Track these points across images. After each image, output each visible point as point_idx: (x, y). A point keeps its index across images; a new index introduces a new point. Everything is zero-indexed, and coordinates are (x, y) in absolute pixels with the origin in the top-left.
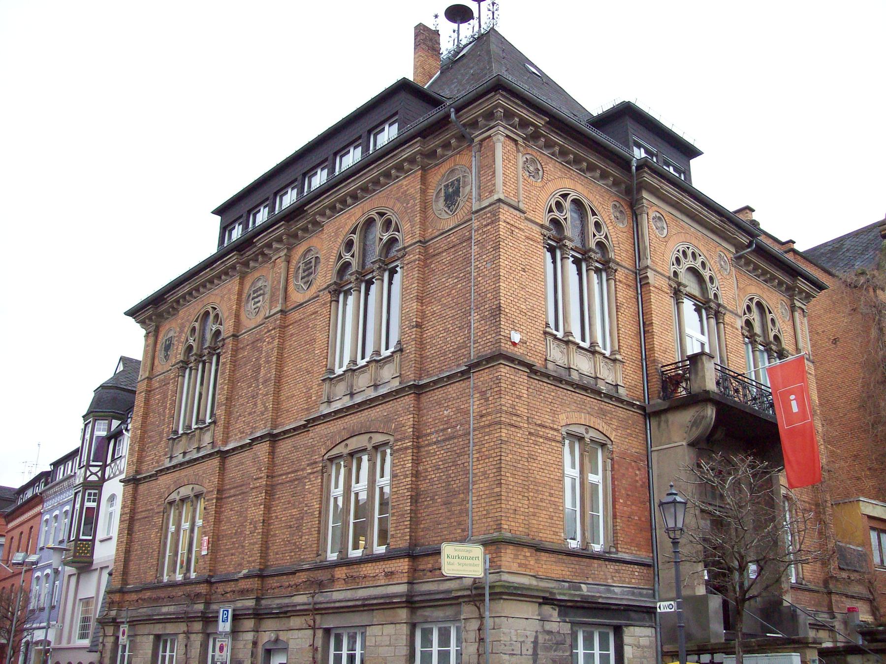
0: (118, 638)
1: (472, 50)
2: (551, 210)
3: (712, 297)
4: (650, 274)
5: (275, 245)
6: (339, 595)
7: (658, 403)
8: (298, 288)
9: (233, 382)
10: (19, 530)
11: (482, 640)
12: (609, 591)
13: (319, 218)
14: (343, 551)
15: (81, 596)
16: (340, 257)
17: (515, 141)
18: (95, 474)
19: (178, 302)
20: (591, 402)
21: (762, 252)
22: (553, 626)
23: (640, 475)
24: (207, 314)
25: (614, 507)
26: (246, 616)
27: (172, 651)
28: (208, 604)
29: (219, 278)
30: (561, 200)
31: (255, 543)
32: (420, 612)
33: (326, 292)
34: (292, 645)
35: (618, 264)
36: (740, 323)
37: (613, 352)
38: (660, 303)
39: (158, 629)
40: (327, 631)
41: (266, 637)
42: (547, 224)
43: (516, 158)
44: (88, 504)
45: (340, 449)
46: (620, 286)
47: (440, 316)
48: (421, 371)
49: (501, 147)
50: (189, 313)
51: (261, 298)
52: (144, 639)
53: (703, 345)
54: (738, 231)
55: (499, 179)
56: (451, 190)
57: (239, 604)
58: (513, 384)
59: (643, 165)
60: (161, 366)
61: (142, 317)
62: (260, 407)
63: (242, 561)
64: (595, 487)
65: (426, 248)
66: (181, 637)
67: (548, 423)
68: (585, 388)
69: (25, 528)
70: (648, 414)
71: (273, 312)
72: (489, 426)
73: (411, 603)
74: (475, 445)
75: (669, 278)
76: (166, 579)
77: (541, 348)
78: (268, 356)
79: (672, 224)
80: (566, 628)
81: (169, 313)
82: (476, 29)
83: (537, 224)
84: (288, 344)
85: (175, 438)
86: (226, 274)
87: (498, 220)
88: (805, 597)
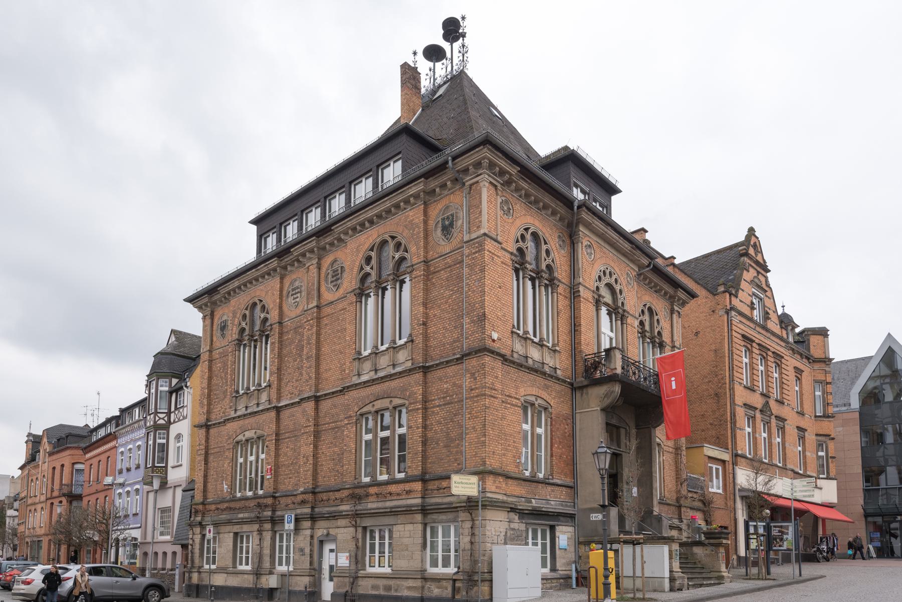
1: (447, 91)
2: (517, 241)
3: (620, 305)
4: (581, 289)
5: (308, 255)
6: (372, 505)
7: (581, 380)
8: (328, 289)
9: (280, 357)
10: (98, 459)
11: (473, 534)
12: (548, 504)
13: (342, 236)
14: (373, 475)
15: (160, 505)
16: (362, 269)
17: (496, 186)
18: (163, 419)
19: (229, 293)
20: (540, 380)
21: (657, 270)
22: (515, 526)
23: (568, 429)
24: (255, 304)
25: (551, 449)
26: (305, 519)
28: (274, 511)
29: (263, 277)
30: (524, 233)
31: (307, 471)
32: (429, 516)
33: (352, 294)
34: (339, 537)
35: (560, 281)
36: (637, 323)
37: (553, 345)
38: (586, 309)
39: (236, 529)
40: (365, 528)
41: (320, 533)
42: (515, 252)
43: (496, 200)
44: (158, 441)
45: (369, 408)
46: (560, 297)
47: (440, 318)
48: (426, 357)
49: (486, 192)
50: (240, 302)
51: (299, 295)
52: (226, 535)
53: (611, 339)
54: (634, 246)
55: (485, 217)
56: (447, 223)
57: (299, 511)
59: (583, 205)
60: (219, 342)
61: (199, 303)
62: (305, 376)
63: (298, 480)
64: (539, 436)
65: (428, 267)
66: (255, 534)
68: (536, 371)
69: (103, 457)
70: (575, 388)
71: (310, 306)
72: (477, 396)
73: (425, 511)
74: (467, 408)
75: (593, 292)
78: (309, 339)
79: (598, 251)
80: (522, 527)
81: (221, 301)
82: (449, 69)
84: (323, 331)
85: (237, 396)
86: (269, 274)
88: (666, 508)
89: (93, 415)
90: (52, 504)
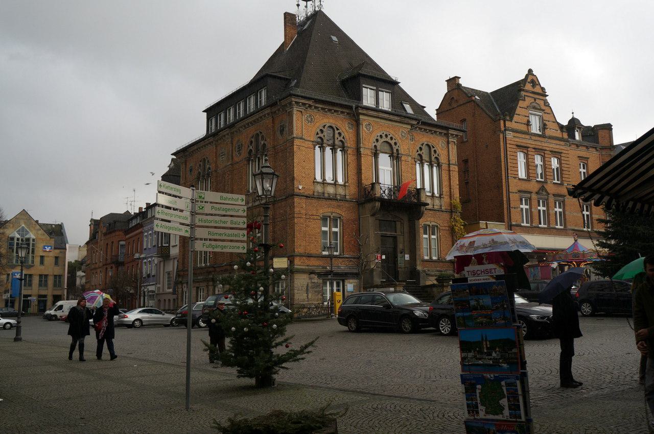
0: (183, 289)
17: (301, 112)
19: (192, 152)
25: (343, 240)
27: (203, 293)
46: (349, 156)
58: (299, 203)
67: (315, 214)
76: (199, 265)
77: (312, 187)
80: (321, 281)
83: (310, 141)
87: (293, 145)
89: (131, 205)
90: (107, 268)
